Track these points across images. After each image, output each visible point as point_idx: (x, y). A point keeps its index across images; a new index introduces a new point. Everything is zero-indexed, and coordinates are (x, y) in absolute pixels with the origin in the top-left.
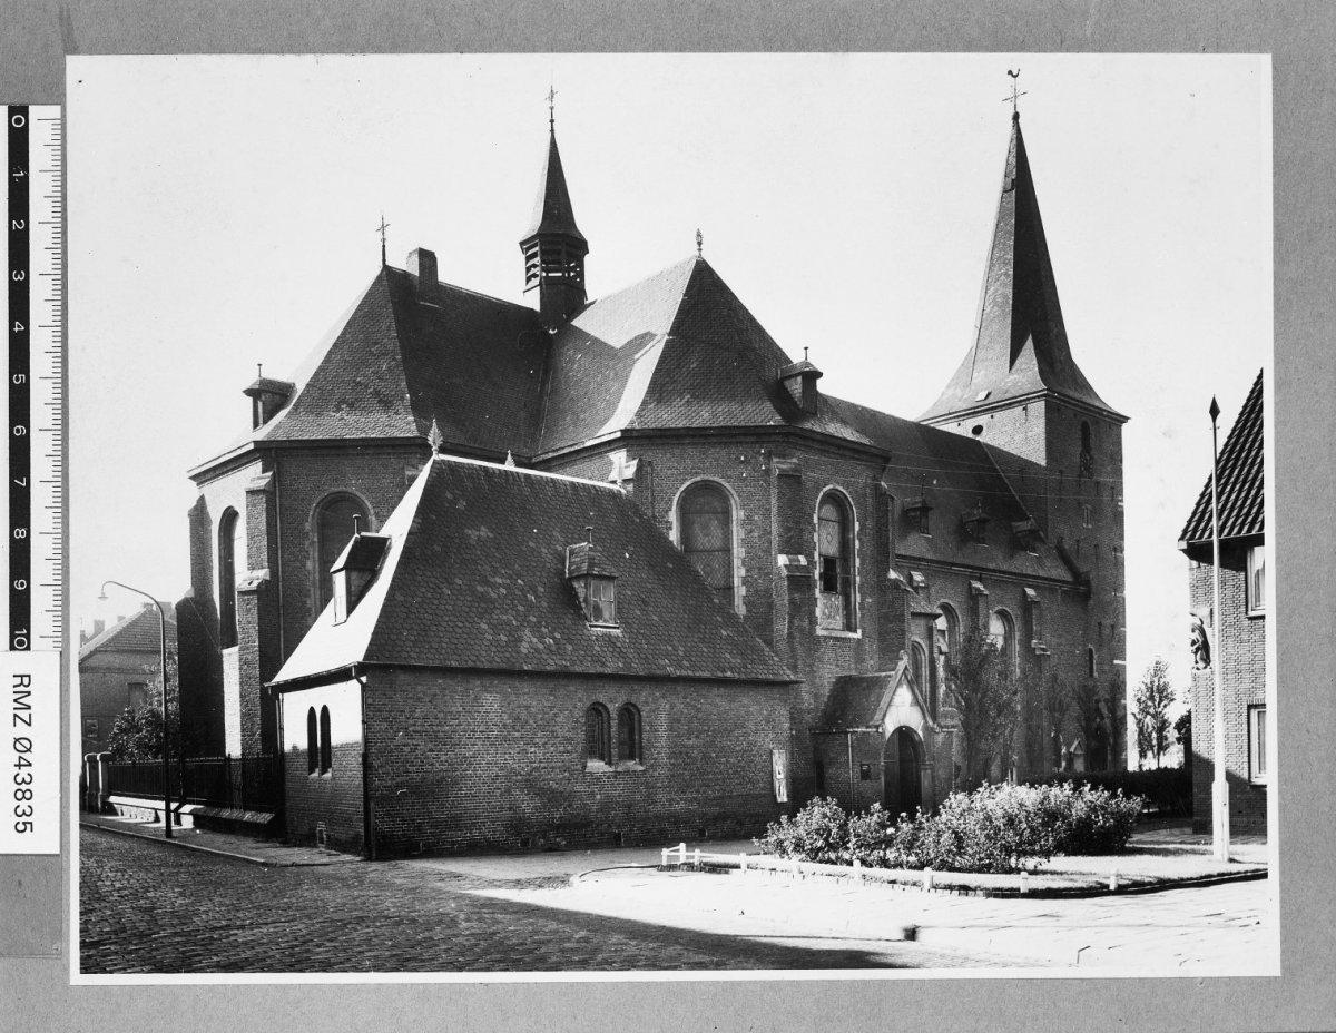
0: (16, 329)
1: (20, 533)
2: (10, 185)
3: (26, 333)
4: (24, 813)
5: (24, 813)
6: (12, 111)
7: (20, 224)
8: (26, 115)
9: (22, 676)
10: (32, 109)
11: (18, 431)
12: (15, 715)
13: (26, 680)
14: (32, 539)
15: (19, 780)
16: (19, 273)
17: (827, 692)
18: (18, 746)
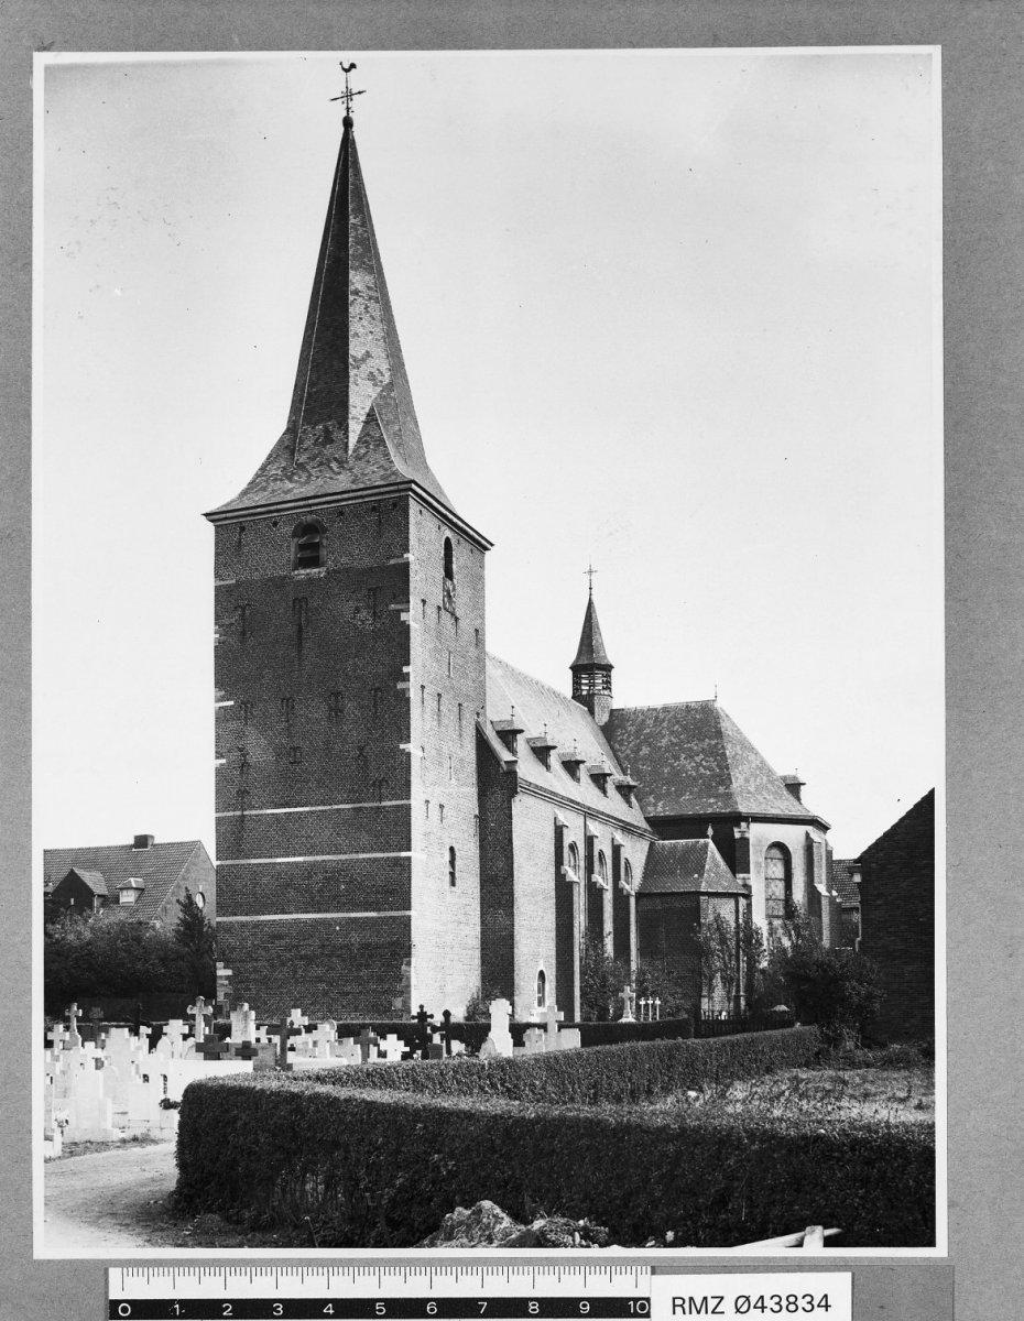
0: (331, 1312)
1: (533, 1307)
3: (335, 1302)
4: (810, 1303)
5: (810, 1303)
7: (228, 1307)
9: (674, 1306)
11: (432, 1310)
12: (713, 1312)
13: (679, 1302)
15: (777, 1308)
16: (275, 1309)
18: (743, 1299)
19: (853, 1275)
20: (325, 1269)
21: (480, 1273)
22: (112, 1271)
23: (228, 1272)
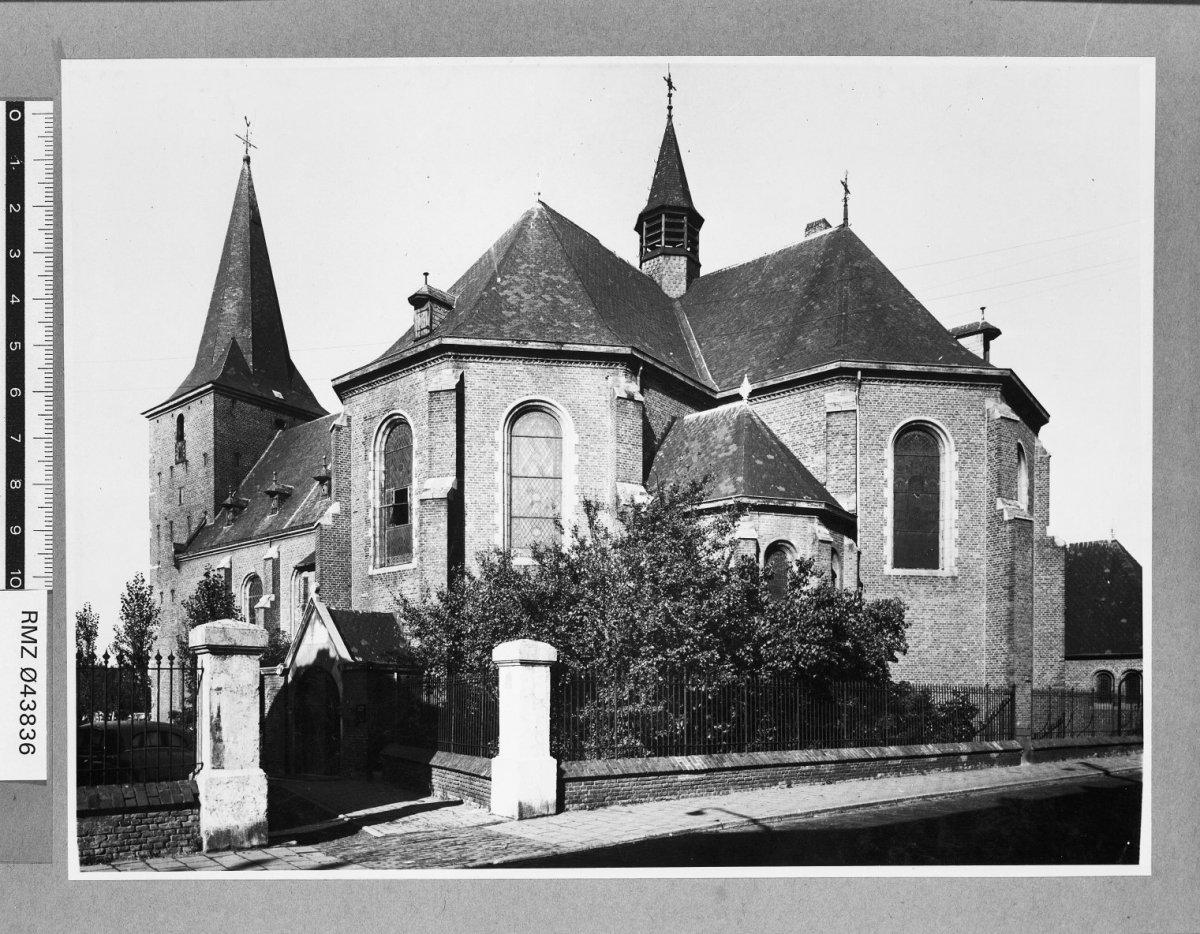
0: (13, 302)
1: (16, 484)
2: (7, 173)
4: (28, 736)
5: (28, 736)
6: (10, 106)
7: (17, 208)
9: (30, 613)
10: (28, 105)
11: (14, 392)
12: (23, 648)
13: (33, 617)
15: (24, 706)
16: (15, 251)
18: (24, 674)
19: (43, 783)
20: (51, 297)
21: (46, 436)
22: (51, 103)
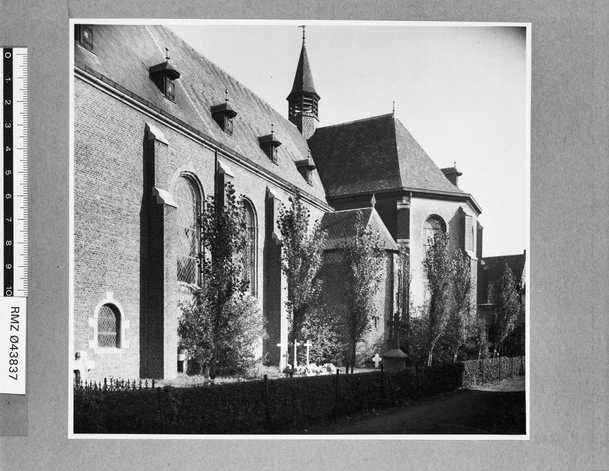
0: (7, 150)
1: (9, 243)
4: (14, 370)
5: (14, 370)
6: (5, 50)
7: (9, 102)
8: (11, 52)
9: (15, 308)
10: (14, 50)
11: (8, 196)
12: (12, 326)
13: (17, 310)
14: (14, 246)
15: (12, 355)
16: (8, 124)
17: (326, 202)
21: (25, 265)
23: (25, 102)
